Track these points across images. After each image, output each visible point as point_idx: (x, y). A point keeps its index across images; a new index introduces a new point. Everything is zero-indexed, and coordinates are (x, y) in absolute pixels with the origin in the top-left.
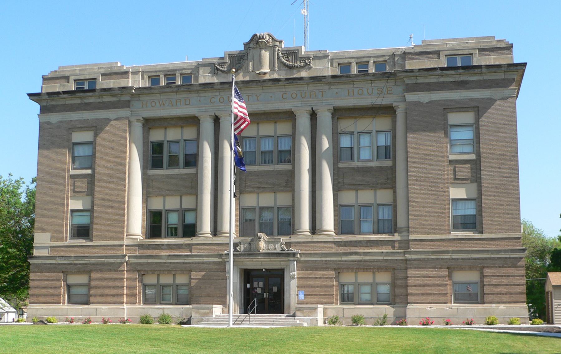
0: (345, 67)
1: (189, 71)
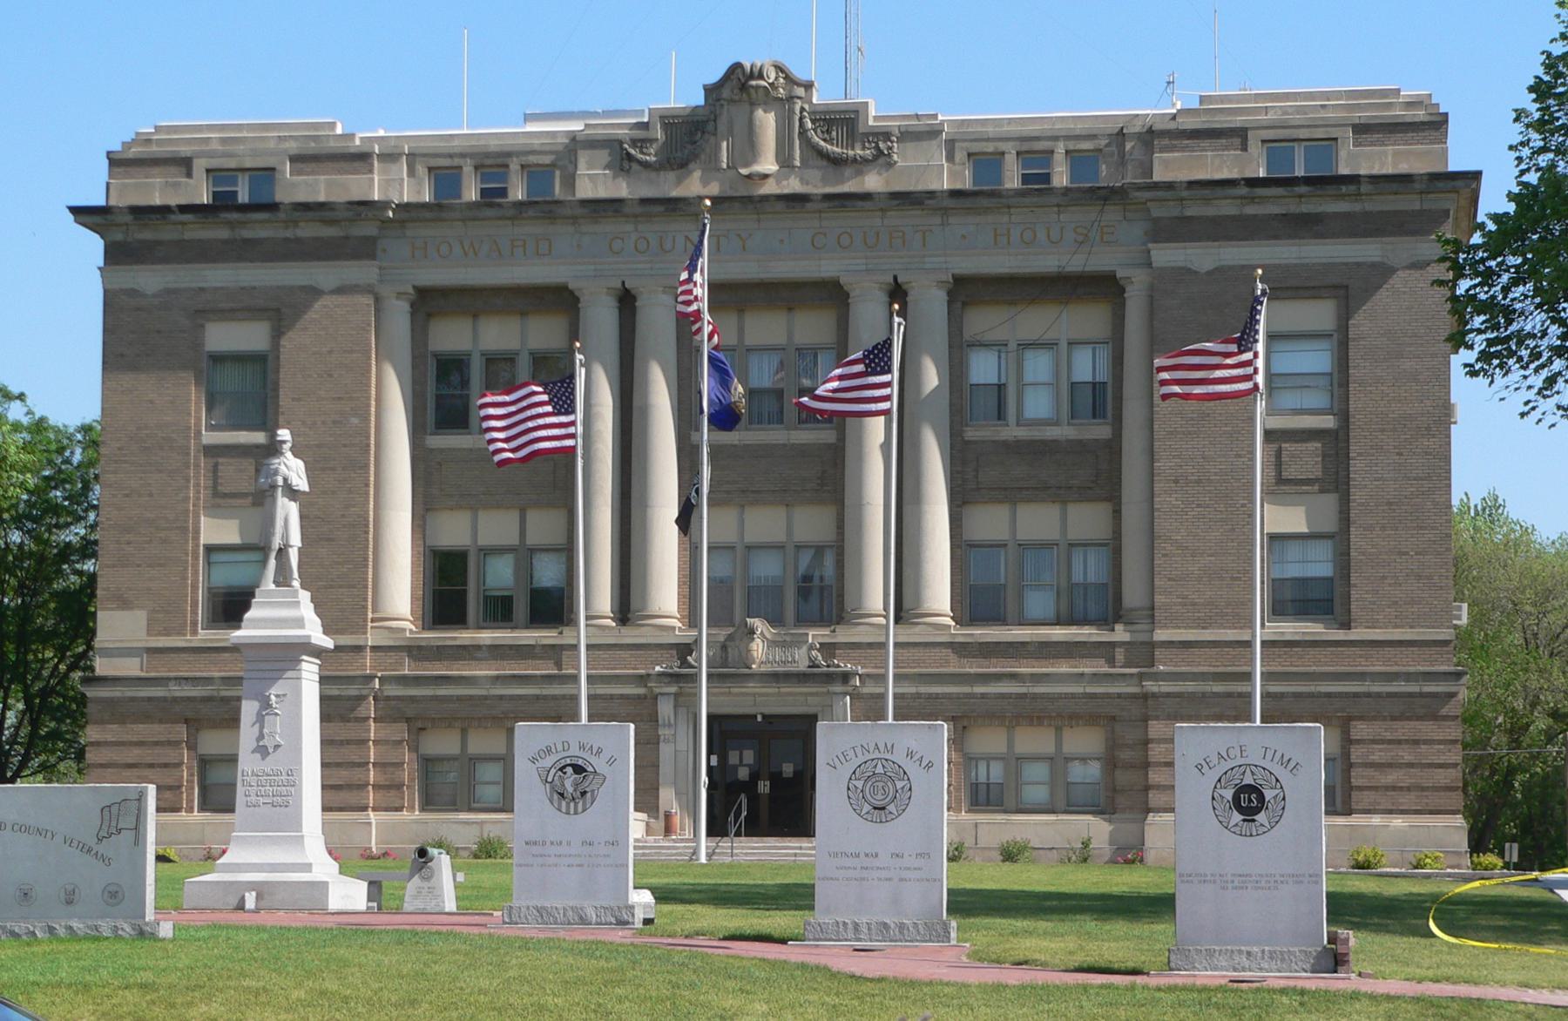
0: (986, 162)
1: (547, 160)
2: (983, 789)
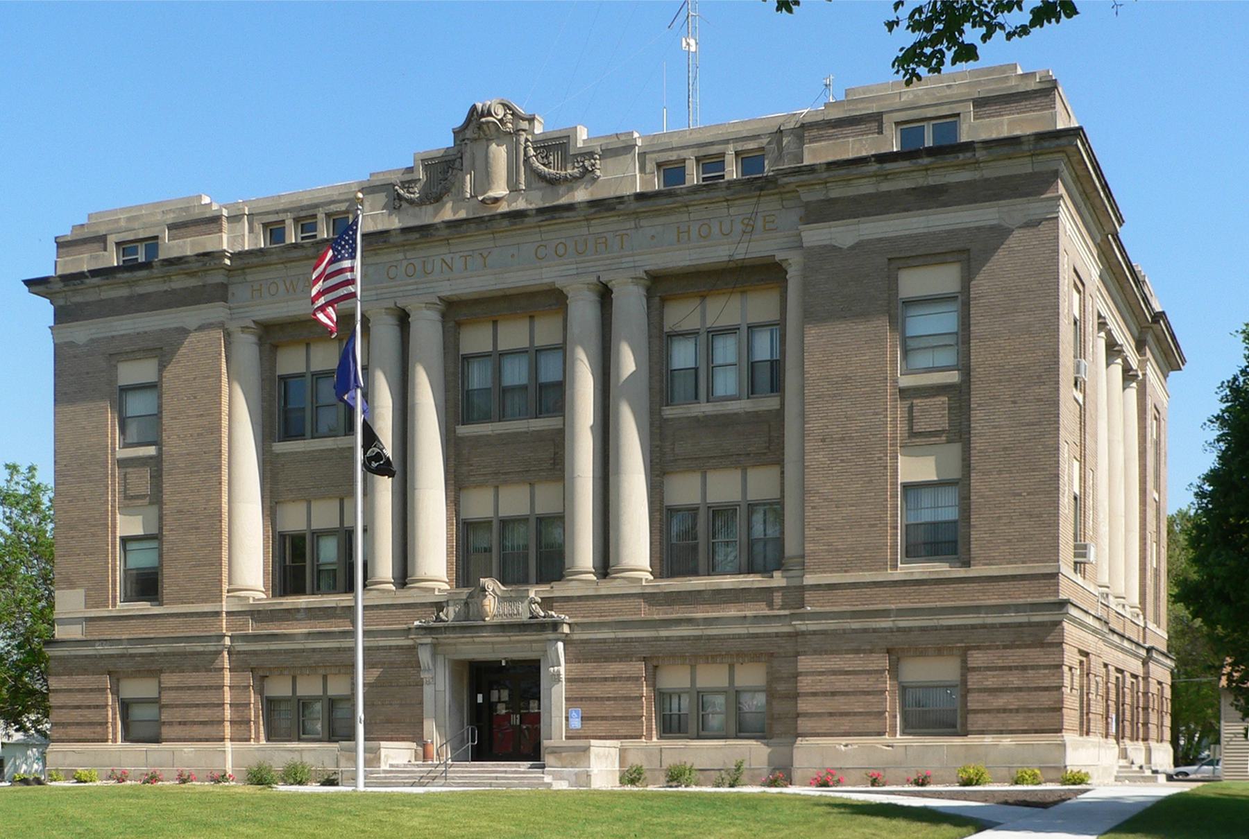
0: (672, 171)
1: (343, 207)
2: (675, 718)
